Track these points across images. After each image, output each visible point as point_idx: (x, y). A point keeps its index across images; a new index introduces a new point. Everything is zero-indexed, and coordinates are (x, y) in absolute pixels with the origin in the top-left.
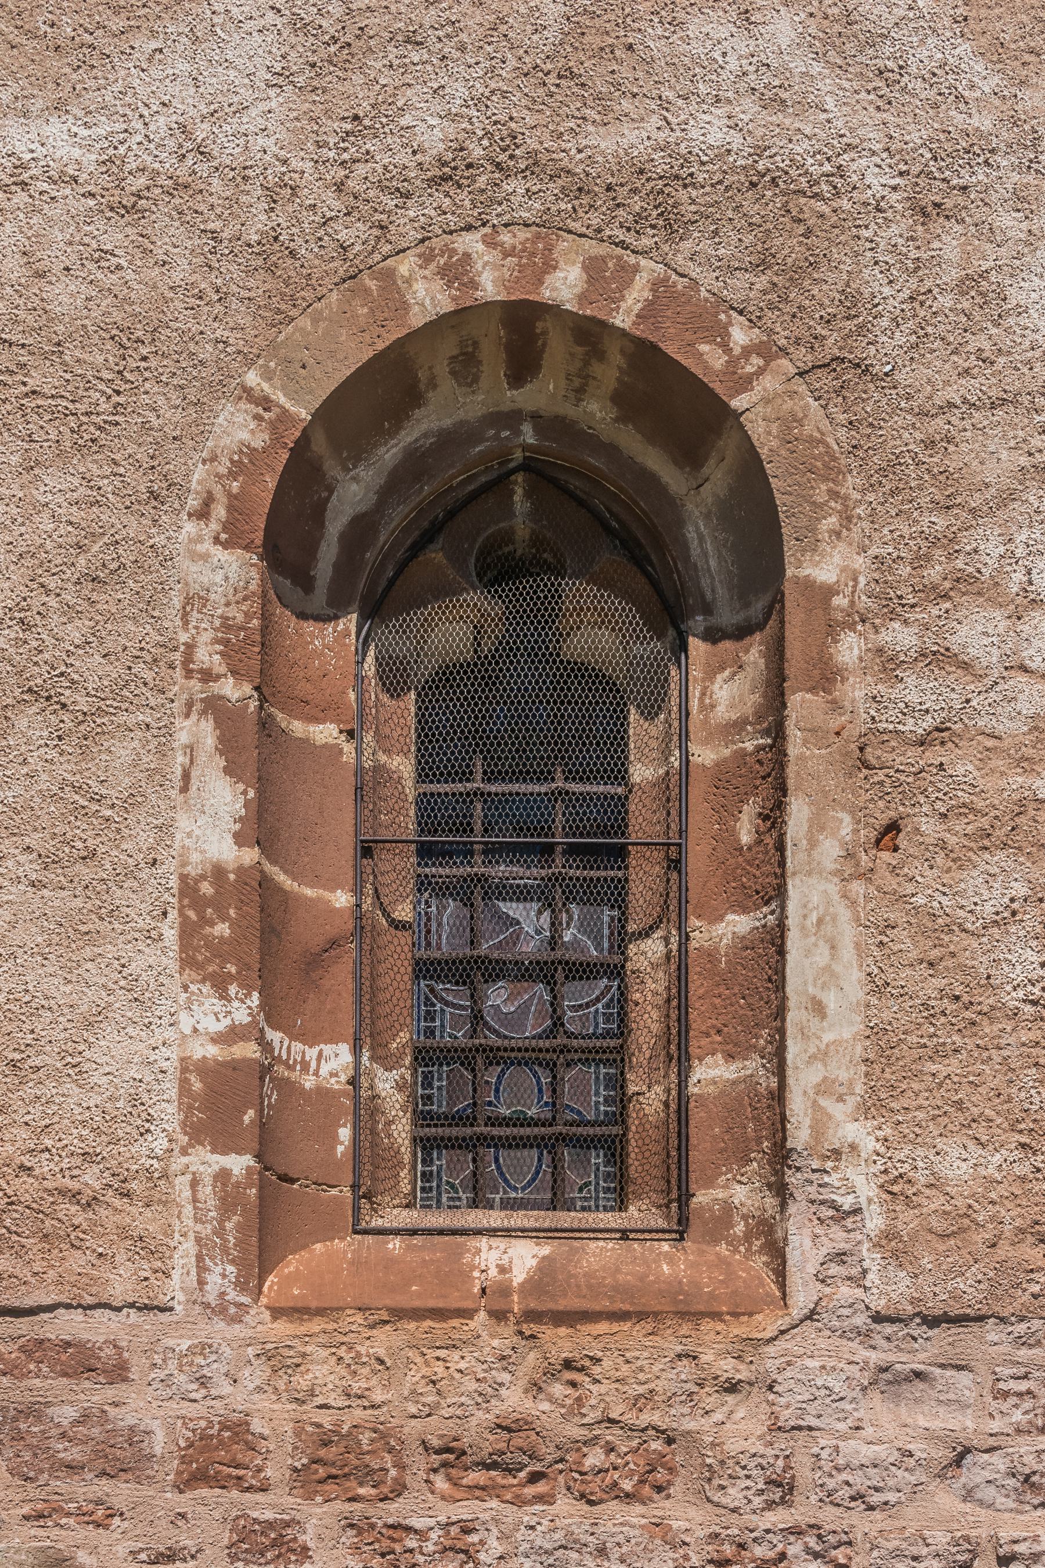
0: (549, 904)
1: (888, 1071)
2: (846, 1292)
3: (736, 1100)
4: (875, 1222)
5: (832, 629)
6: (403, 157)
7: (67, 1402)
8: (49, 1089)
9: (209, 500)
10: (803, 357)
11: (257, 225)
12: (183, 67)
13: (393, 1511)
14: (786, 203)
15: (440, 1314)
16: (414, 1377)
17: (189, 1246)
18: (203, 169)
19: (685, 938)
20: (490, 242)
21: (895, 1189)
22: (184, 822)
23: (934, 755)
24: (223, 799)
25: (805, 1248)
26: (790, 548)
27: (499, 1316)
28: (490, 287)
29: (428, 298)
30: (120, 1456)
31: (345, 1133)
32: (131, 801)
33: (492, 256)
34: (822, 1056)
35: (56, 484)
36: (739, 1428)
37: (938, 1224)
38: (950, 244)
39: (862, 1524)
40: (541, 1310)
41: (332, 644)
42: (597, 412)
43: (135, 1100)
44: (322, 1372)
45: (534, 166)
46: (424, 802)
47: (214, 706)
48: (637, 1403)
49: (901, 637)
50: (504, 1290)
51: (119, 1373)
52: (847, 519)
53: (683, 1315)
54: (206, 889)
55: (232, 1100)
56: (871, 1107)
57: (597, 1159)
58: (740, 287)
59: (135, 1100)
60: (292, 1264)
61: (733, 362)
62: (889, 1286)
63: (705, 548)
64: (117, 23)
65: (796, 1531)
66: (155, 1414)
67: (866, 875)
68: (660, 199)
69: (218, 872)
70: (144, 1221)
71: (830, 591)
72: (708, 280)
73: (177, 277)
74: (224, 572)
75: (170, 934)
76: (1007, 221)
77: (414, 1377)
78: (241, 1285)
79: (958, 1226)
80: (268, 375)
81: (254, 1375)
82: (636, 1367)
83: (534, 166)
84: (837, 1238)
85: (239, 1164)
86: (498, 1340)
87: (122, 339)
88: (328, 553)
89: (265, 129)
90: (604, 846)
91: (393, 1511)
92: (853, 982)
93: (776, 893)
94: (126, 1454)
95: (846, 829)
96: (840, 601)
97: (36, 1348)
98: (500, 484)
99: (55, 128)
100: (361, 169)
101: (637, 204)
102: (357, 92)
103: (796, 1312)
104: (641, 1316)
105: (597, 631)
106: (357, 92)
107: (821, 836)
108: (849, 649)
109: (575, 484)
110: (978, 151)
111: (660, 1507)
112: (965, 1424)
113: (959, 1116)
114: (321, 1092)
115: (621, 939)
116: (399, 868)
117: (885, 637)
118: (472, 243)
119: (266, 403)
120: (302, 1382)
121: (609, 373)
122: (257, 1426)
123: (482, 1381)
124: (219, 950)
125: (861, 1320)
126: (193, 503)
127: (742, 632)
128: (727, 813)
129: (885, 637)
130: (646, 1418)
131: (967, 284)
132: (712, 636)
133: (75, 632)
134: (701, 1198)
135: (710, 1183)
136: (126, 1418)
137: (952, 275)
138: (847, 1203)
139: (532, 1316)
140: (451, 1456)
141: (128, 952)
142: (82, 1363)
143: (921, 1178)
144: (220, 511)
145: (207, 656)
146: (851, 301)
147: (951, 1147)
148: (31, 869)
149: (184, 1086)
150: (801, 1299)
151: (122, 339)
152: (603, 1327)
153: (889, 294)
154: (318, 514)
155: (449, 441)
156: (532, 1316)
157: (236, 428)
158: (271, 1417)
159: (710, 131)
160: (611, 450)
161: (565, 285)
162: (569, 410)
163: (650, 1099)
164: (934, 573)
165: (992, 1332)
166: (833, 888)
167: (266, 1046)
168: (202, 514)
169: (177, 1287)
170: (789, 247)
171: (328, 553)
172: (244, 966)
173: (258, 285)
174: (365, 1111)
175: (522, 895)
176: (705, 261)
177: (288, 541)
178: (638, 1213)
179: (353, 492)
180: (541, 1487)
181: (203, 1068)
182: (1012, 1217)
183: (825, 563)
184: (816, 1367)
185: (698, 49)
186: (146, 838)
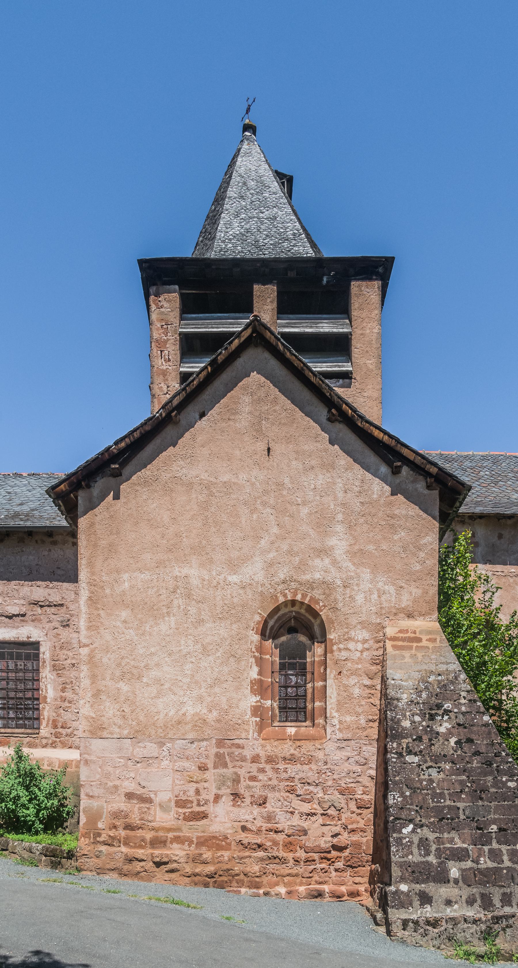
0: (296, 676)
1: (340, 705)
2: (334, 736)
3: (320, 708)
4: (338, 727)
5: (333, 645)
6: (278, 580)
7: (237, 752)
8: (234, 709)
9: (254, 628)
10: (329, 607)
11: (260, 589)
12: (250, 568)
13: (277, 766)
14: (327, 586)
15: (283, 740)
16: (280, 748)
17: (252, 731)
18: (253, 582)
19: (314, 685)
20: (289, 591)
21: (340, 722)
22: (251, 673)
23: (346, 662)
24: (256, 669)
25: (329, 730)
26: (327, 633)
27: (290, 740)
28: (289, 598)
29: (281, 599)
30: (243, 759)
31: (270, 713)
32: (244, 670)
33: (290, 593)
34: (331, 704)
35: (235, 626)
36: (320, 755)
37: (346, 727)
38: (348, 591)
39: (336, 768)
40: (296, 739)
41: (269, 644)
42: (303, 611)
43: (245, 711)
44: (268, 748)
45: (295, 581)
46: (280, 663)
47: (254, 656)
48: (308, 751)
49: (341, 646)
50: (291, 736)
51: (243, 748)
52: (335, 629)
53: (313, 739)
54: (254, 682)
55: (257, 710)
56: (337, 711)
57: (303, 713)
58: (322, 597)
59: (245, 711)
60: (264, 732)
61: (320, 608)
62: (339, 736)
63: (317, 630)
64: (242, 562)
65: (328, 769)
66: (248, 753)
67: (337, 679)
68: (311, 585)
69: (255, 679)
70: (246, 727)
71: (333, 639)
72: (317, 596)
73: (250, 597)
74: (256, 638)
75: (249, 688)
76: (355, 588)
77: (280, 748)
78: (258, 736)
79: (348, 727)
80: (261, 610)
81: (260, 748)
82: (307, 746)
83: (295, 581)
84: (333, 729)
85: (258, 719)
86: (290, 743)
87: (243, 606)
88: (268, 631)
89: (260, 577)
90: (303, 667)
91: (277, 766)
92: (335, 693)
93: (326, 680)
94: (244, 758)
95: (334, 673)
96: (334, 641)
97: (233, 745)
98: (291, 619)
99: (234, 577)
100: (273, 582)
101: (308, 586)
102: (272, 571)
103: (328, 739)
104: (308, 740)
105: (302, 638)
106: (272, 571)
107: (331, 674)
108: (335, 648)
109: (300, 620)
110: (352, 578)
111: (311, 766)
112: (349, 754)
113: (348, 712)
114: (267, 707)
115: (306, 683)
116: (276, 675)
117: (339, 646)
118: (287, 591)
119: (261, 614)
120: (266, 749)
121: (304, 607)
122: (260, 755)
123: (288, 748)
124: (255, 690)
125: (336, 740)
126: (252, 628)
127: (321, 642)
128: (319, 667)
129: (339, 646)
130: (309, 754)
131: (350, 597)
132: (318, 642)
133: (237, 647)
134: (316, 722)
135: (317, 719)
136: (244, 754)
137: (348, 595)
138: (334, 724)
139: (294, 740)
140: (285, 759)
141: (244, 690)
142: (238, 746)
143: (344, 721)
144: (255, 630)
145: (254, 650)
146: (335, 600)
147: (347, 716)
148: (232, 680)
149: (251, 709)
150: (328, 737)
151: (243, 606)
152: (303, 741)
153: (340, 598)
154: (267, 627)
155: (284, 615)
156: (294, 740)
157: (257, 618)
158: (262, 754)
159: (317, 576)
160: (305, 616)
161: (299, 597)
162: (299, 611)
163: (309, 706)
164: (346, 637)
165: (352, 742)
166: (333, 681)
167: (261, 702)
168: (253, 630)
169: (250, 737)
170: (327, 591)
171: (268, 631)
172: (258, 692)
173: (260, 598)
174: (272, 709)
175: (292, 675)
176: (317, 594)
177: (263, 634)
178: (308, 723)
179: (271, 623)
180: (296, 763)
181: (253, 706)
182: (355, 726)
183: (332, 636)
184: (330, 747)
185: (316, 564)
186: (246, 675)
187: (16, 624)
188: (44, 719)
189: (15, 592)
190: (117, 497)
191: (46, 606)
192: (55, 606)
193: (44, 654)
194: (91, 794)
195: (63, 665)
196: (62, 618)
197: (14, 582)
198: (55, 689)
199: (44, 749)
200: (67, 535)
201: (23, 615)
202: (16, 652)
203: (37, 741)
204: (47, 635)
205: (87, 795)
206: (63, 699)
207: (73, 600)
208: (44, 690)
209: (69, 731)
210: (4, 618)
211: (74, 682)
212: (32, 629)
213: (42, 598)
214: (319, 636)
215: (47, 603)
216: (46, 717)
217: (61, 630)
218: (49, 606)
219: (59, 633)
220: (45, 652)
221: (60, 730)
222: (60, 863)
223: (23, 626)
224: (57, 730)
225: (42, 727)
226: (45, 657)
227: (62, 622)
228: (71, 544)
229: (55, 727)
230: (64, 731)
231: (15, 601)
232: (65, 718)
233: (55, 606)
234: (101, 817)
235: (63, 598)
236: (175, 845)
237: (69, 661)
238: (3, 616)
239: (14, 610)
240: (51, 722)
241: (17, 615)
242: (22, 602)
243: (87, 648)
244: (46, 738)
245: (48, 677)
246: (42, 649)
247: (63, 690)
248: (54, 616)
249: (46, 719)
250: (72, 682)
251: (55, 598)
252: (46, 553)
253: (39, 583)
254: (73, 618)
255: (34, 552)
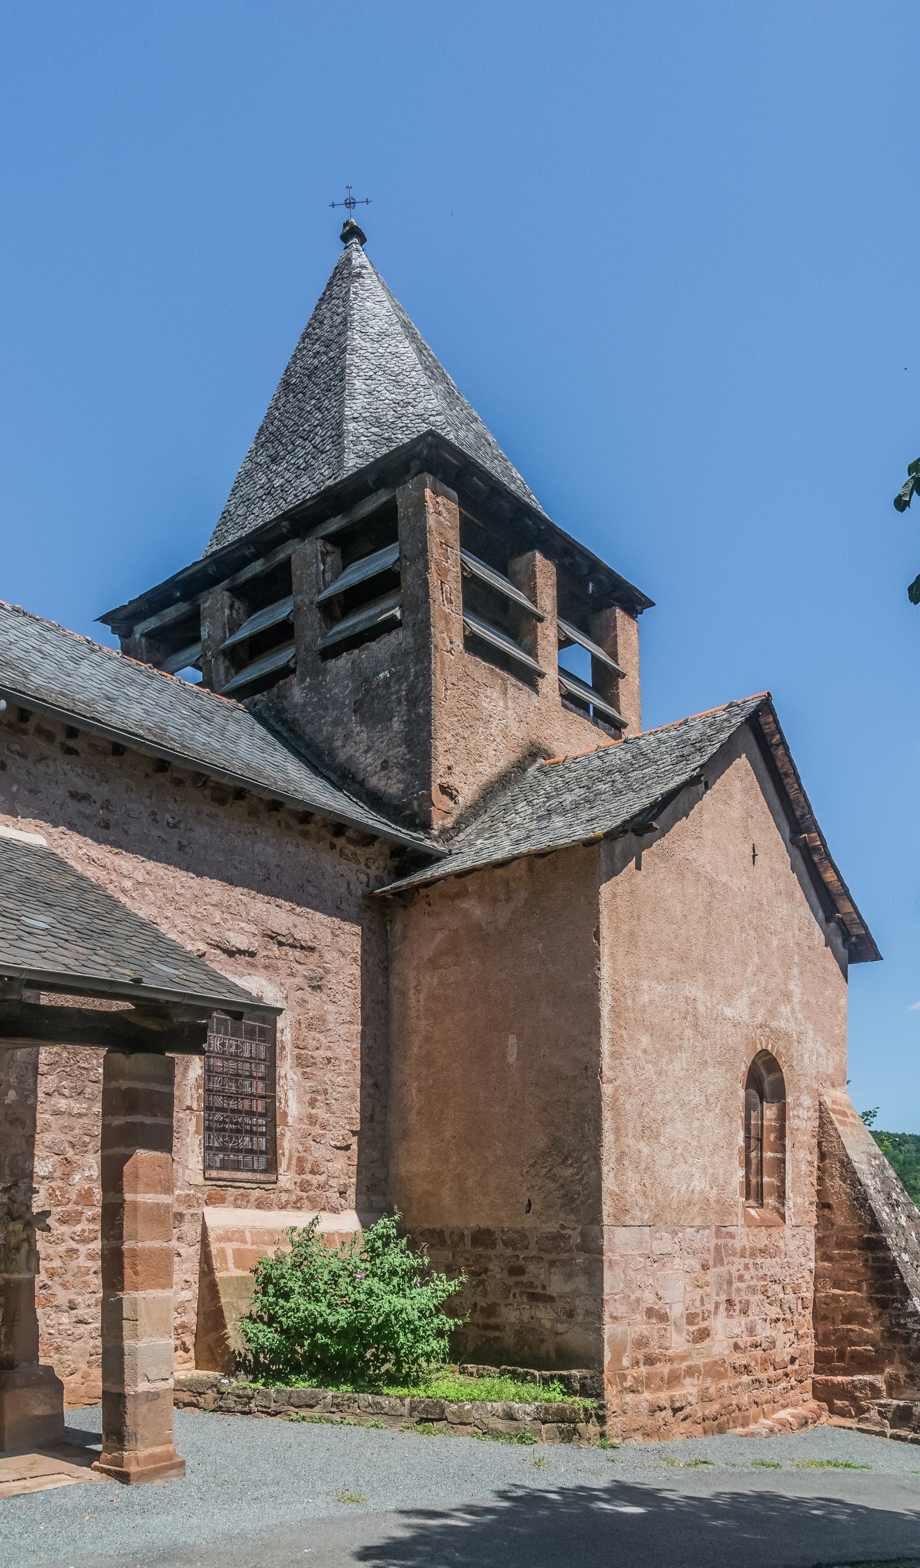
132: (767, 1102)
187: (240, 969)
188: (283, 1154)
189: (242, 907)
190: (638, 867)
191: (288, 945)
192: (302, 948)
193: (282, 1033)
194: (615, 1315)
195: (312, 1057)
196: (311, 972)
197: (239, 890)
198: (299, 1101)
199: (283, 1212)
200: (324, 826)
201: (252, 954)
202: (260, 1027)
203: (272, 1196)
204: (286, 998)
205: (612, 1317)
206: (312, 1120)
207: (328, 944)
208: (283, 1101)
209: (322, 1178)
210: (218, 952)
211: (330, 1091)
212: (264, 982)
213: (284, 929)
214: (768, 1095)
215: (291, 941)
216: (287, 1152)
217: (308, 994)
218: (292, 946)
219: (306, 998)
220: (286, 1030)
221: (309, 1177)
222: (575, 1431)
223: (250, 974)
224: (303, 1176)
225: (281, 1171)
226: (284, 1038)
227: (311, 979)
228: (328, 845)
229: (301, 1171)
230: (315, 1180)
231: (243, 925)
232: (317, 1155)
233: (302, 948)
234: (625, 1350)
235: (315, 937)
236: (688, 1381)
237: (322, 1053)
238: (218, 947)
239: (239, 941)
240: (294, 1162)
241: (241, 952)
242: (253, 928)
243: (611, 1085)
244: (287, 1191)
245: (289, 1077)
246: (281, 1023)
247: (312, 1103)
248: (298, 967)
249: (287, 1156)
250: (325, 1092)
251: (303, 934)
252: (292, 849)
253: (280, 901)
254: (329, 977)
255: (274, 840)
